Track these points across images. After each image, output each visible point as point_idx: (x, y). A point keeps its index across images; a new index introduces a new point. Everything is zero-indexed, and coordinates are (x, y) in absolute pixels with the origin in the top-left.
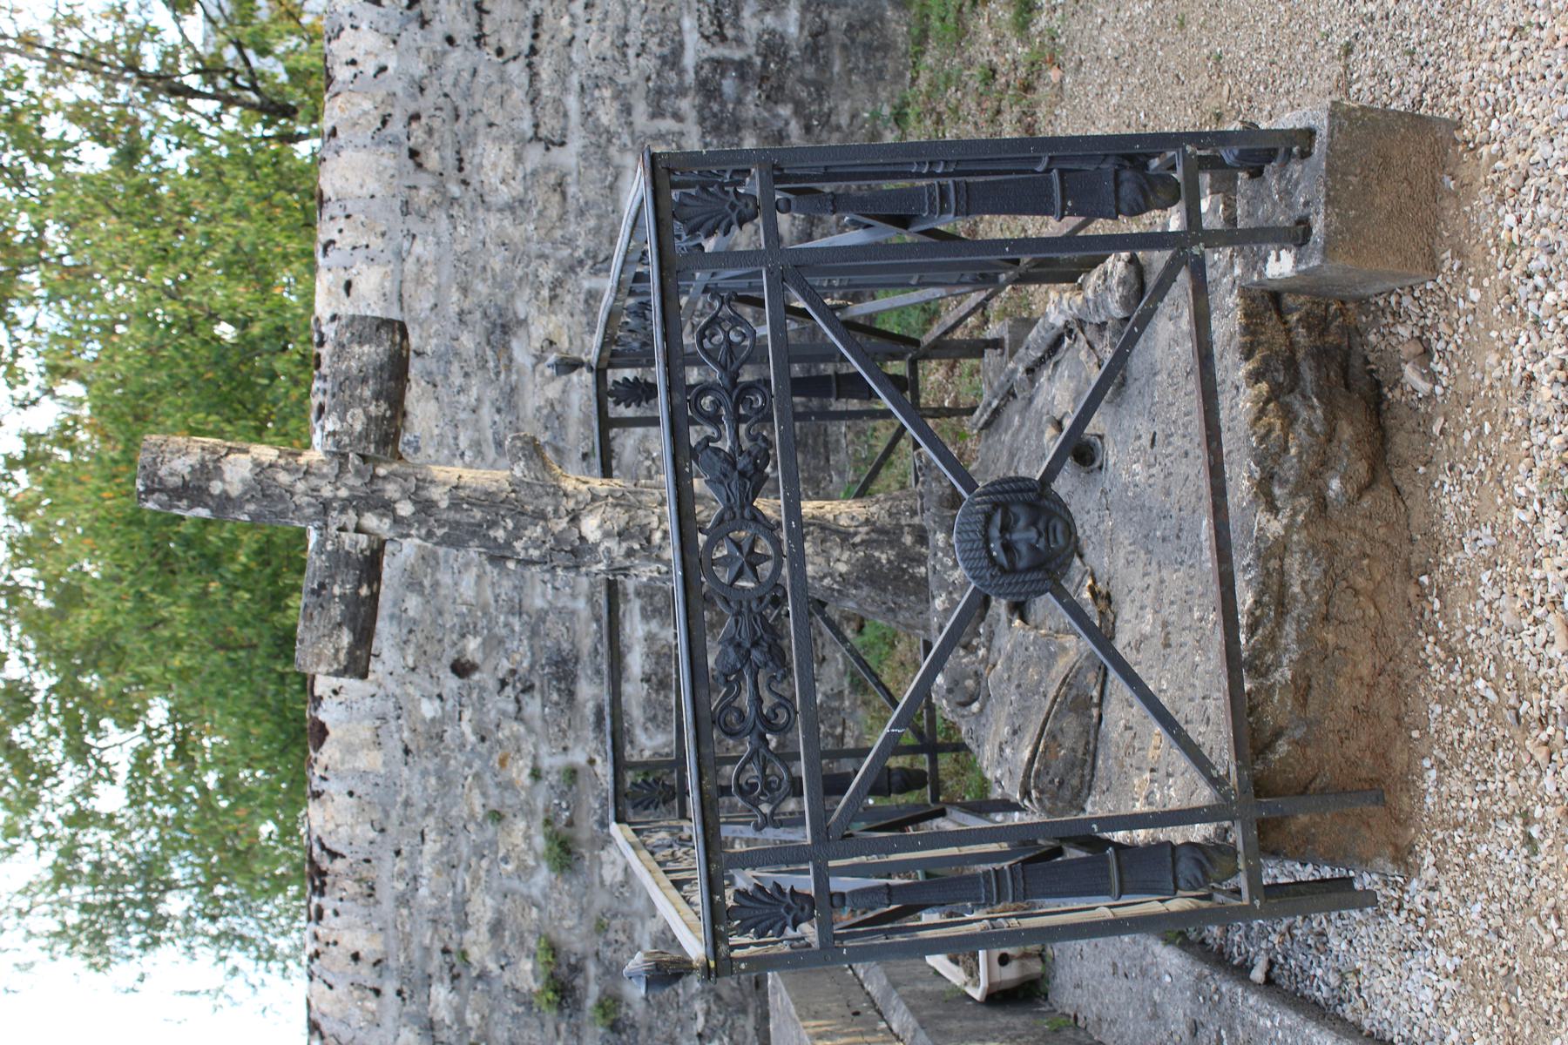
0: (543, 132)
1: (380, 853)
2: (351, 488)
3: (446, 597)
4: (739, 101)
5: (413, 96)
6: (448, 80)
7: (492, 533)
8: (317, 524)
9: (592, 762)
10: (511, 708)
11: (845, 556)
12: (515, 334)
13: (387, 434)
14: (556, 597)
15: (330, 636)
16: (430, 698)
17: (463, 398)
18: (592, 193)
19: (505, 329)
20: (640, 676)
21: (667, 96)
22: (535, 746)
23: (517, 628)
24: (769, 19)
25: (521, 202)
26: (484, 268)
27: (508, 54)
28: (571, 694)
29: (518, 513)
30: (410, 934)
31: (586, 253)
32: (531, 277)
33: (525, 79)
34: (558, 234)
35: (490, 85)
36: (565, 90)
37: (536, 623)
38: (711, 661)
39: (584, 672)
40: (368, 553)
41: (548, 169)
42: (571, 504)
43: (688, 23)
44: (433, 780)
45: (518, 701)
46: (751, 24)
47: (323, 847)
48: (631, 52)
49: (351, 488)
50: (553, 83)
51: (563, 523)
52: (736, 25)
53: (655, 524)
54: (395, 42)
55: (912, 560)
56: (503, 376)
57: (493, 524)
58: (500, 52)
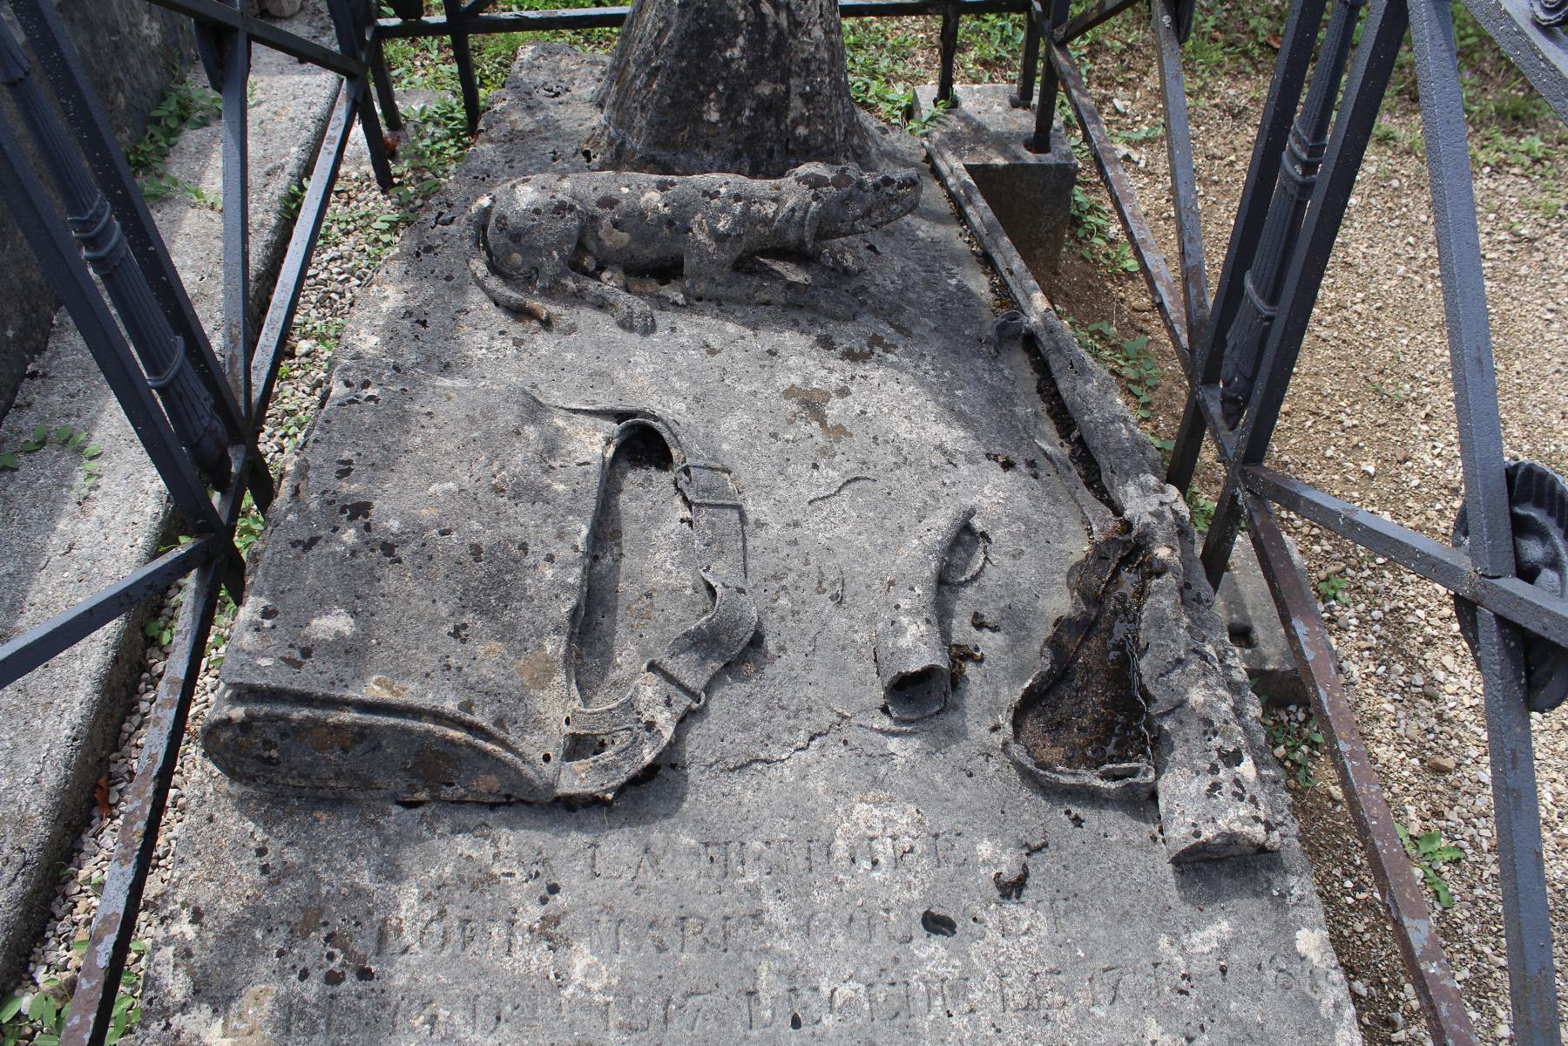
38: (233, 470)
55: (730, 100)
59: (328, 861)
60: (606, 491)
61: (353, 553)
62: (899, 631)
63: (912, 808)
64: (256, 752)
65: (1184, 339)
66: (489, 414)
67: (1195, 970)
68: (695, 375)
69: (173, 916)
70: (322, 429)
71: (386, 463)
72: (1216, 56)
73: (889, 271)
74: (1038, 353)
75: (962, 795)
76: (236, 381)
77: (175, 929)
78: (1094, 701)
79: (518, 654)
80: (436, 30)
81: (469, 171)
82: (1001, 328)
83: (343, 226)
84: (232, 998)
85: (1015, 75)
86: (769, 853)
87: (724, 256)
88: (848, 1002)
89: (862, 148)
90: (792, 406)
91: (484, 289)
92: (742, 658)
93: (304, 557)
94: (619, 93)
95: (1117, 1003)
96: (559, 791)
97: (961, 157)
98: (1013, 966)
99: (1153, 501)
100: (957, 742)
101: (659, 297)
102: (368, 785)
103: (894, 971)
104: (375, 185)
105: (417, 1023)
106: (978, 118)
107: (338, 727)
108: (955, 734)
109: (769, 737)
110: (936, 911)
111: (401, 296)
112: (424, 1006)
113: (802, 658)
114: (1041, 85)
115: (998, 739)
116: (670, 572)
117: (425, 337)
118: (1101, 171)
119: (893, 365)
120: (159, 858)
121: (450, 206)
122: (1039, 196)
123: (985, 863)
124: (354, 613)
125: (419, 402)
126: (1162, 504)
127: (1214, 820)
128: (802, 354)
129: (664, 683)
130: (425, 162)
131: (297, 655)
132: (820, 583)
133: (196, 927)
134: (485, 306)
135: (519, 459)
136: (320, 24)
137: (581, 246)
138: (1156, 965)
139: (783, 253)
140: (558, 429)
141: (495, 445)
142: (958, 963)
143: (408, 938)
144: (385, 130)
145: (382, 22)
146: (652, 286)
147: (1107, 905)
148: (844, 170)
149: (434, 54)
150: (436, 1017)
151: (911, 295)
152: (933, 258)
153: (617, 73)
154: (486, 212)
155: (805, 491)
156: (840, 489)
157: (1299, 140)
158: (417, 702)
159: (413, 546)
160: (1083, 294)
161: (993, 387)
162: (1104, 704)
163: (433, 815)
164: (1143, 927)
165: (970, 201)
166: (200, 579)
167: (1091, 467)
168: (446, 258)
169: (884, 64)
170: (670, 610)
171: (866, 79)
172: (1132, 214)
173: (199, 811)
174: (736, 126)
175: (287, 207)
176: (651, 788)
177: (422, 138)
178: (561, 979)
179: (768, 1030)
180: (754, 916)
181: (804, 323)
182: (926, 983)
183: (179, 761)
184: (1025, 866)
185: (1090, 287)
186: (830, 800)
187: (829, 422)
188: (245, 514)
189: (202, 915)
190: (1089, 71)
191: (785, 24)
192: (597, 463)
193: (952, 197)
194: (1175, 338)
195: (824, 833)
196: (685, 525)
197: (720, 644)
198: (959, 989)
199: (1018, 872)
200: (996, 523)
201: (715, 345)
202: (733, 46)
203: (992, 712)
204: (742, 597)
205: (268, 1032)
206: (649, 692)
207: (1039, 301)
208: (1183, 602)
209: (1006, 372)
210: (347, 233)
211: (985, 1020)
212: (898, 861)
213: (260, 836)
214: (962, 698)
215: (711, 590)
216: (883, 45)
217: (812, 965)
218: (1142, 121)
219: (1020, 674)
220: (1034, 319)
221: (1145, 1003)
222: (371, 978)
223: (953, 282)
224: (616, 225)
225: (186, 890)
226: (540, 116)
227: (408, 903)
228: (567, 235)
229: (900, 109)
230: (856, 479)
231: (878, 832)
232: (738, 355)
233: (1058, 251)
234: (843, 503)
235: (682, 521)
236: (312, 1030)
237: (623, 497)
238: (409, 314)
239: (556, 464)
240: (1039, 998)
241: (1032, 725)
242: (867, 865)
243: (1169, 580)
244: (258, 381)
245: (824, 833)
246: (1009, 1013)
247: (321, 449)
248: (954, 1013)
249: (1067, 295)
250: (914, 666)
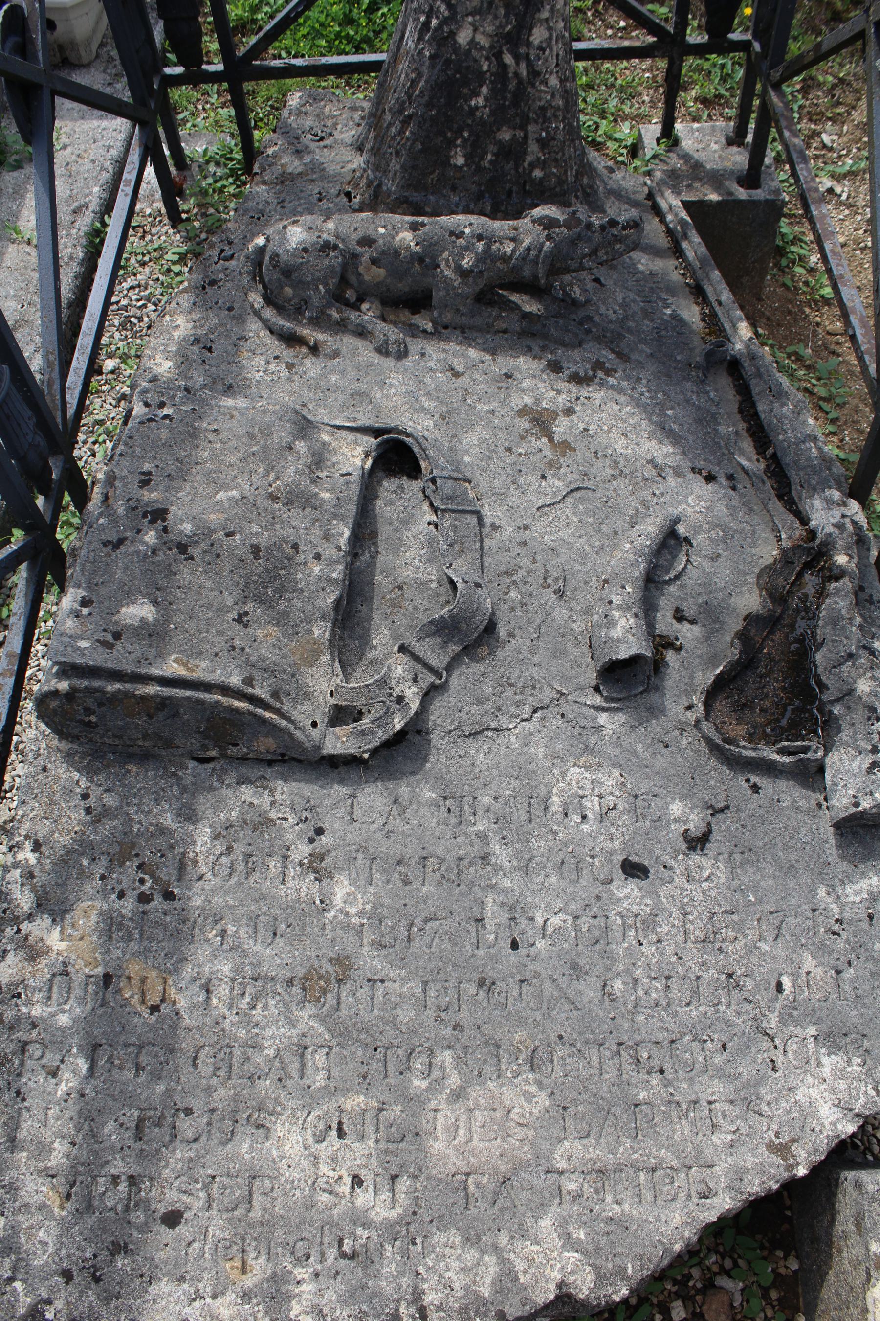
38: (54, 476)
59: (138, 805)
60: (365, 497)
61: (154, 552)
62: (612, 624)
63: (616, 772)
64: (78, 718)
65: (873, 368)
66: (266, 431)
67: (847, 915)
68: (441, 396)
69: (19, 846)
70: (126, 444)
71: (179, 474)
73: (613, 301)
74: (741, 377)
75: (659, 763)
76: (53, 401)
77: (20, 856)
78: (775, 686)
79: (291, 637)
80: (215, 78)
81: (246, 211)
82: (709, 355)
83: (140, 257)
84: (66, 911)
86: (497, 806)
87: (467, 290)
88: (557, 930)
89: (591, 187)
90: (524, 424)
91: (260, 318)
92: (478, 642)
93: (114, 554)
94: (376, 140)
95: (779, 940)
96: (325, 752)
97: (678, 194)
98: (695, 907)
99: (836, 515)
100: (656, 718)
101: (411, 325)
102: (169, 744)
103: (596, 906)
104: (166, 221)
105: (210, 936)
107: (144, 698)
108: (655, 711)
109: (499, 710)
110: (634, 858)
111: (190, 325)
112: (216, 922)
113: (528, 643)
114: (756, 123)
115: (691, 716)
116: (419, 568)
117: (211, 362)
118: (806, 207)
119: (612, 387)
120: (6, 792)
121: (230, 243)
123: (676, 820)
124: (155, 603)
125: (207, 420)
126: (843, 516)
127: (871, 793)
128: (534, 377)
129: (412, 663)
131: (109, 638)
132: (545, 579)
133: (37, 855)
134: (262, 334)
135: (291, 471)
136: (114, 71)
137: (344, 281)
138: (814, 910)
139: (519, 286)
140: (324, 444)
141: (270, 458)
142: (649, 902)
143: (203, 868)
144: (173, 170)
145: (168, 71)
146: (405, 315)
147: (776, 859)
148: (574, 213)
149: (214, 99)
150: (226, 931)
151: (631, 324)
152: (652, 289)
153: (374, 119)
154: (262, 250)
155: (534, 499)
156: (564, 499)
158: (209, 678)
159: (203, 546)
160: (782, 320)
161: (699, 408)
162: (783, 689)
163: (222, 769)
164: (805, 879)
165: (685, 236)
166: (30, 569)
167: (782, 482)
168: (228, 291)
169: (613, 103)
170: (418, 600)
171: (596, 118)
172: (832, 251)
173: (36, 763)
174: (479, 169)
175: (92, 242)
176: (400, 751)
177: (205, 177)
178: (325, 905)
179: (491, 950)
180: (483, 858)
181: (536, 349)
182: (622, 917)
183: (19, 714)
184: (709, 824)
185: (790, 312)
186: (548, 763)
187: (556, 438)
188: (65, 509)
189: (41, 846)
190: (800, 107)
191: (525, 73)
192: (357, 474)
193: (670, 232)
194: (864, 368)
195: (542, 792)
196: (432, 527)
197: (459, 631)
198: (649, 923)
199: (704, 829)
200: (698, 530)
201: (459, 368)
202: (477, 95)
203: (687, 694)
204: (479, 591)
205: (95, 938)
206: (399, 670)
207: (744, 330)
208: (857, 604)
209: (712, 394)
210: (143, 264)
211: (669, 950)
212: (603, 816)
213: (84, 783)
214: (662, 680)
215: (452, 583)
216: (613, 85)
217: (529, 899)
218: (847, 155)
219: (713, 660)
220: (739, 346)
221: (803, 941)
222: (174, 899)
223: (668, 311)
224: (374, 261)
225: (28, 825)
226: (307, 159)
227: (203, 840)
228: (331, 270)
229: (626, 147)
230: (579, 489)
231: (588, 792)
232: (479, 377)
233: (763, 279)
234: (567, 509)
235: (429, 524)
236: (129, 938)
237: (379, 503)
238: (197, 341)
239: (322, 475)
240: (715, 933)
241: (721, 706)
242: (577, 818)
243: (845, 584)
244: (72, 399)
245: (542, 792)
246: (690, 944)
247: (125, 462)
248: (644, 942)
249: (768, 319)
250: (623, 654)
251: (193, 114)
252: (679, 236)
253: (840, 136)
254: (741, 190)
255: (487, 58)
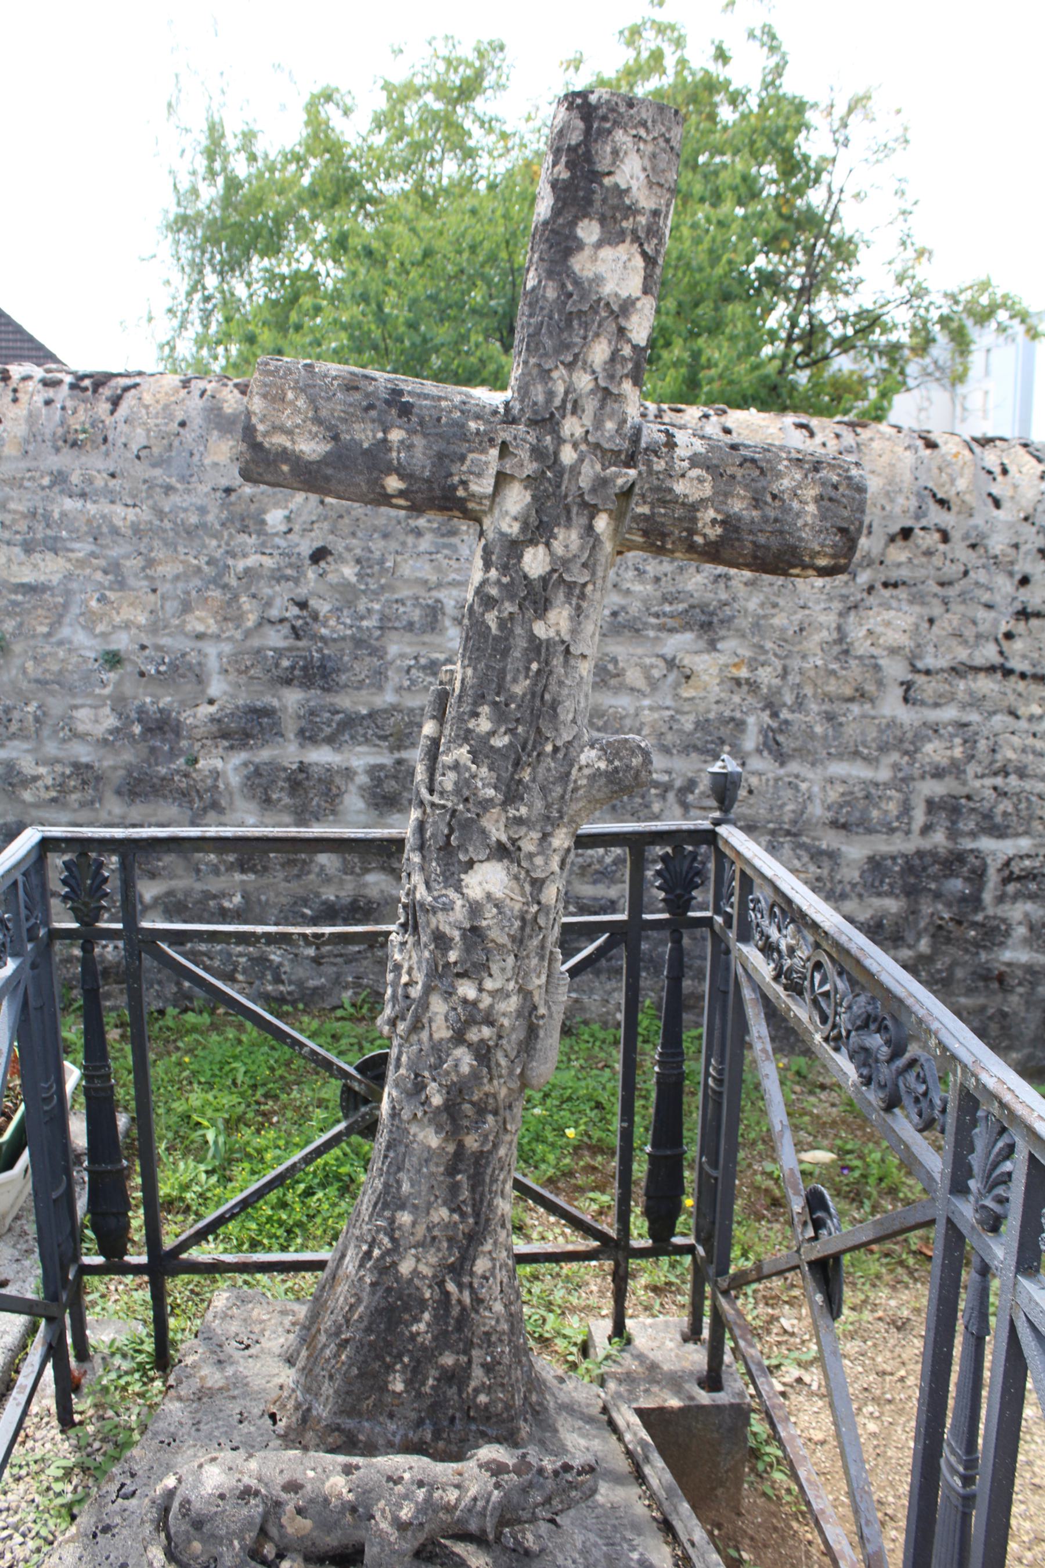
0: (921, 679)
1: (114, 455)
2: (575, 470)
3: (404, 544)
4: (937, 896)
5: (966, 537)
6: (981, 576)
7: (485, 710)
8: (517, 406)
9: (211, 702)
10: (274, 613)
11: (425, 1270)
12: (700, 637)
13: (663, 536)
14: (399, 669)
15: (318, 420)
16: (288, 519)
17: (631, 574)
18: (851, 731)
19: (706, 627)
20: (306, 760)
21: (949, 818)
22: (229, 639)
23: (365, 623)
24: (1022, 931)
25: (846, 652)
26: (775, 605)
27: (1005, 644)
28: (288, 682)
29: (517, 757)
30: (21, 486)
31: (786, 722)
32: (762, 658)
33: (979, 661)
34: (808, 690)
35: (974, 623)
36: (964, 706)
37: (369, 646)
39: (315, 697)
40: (461, 493)
41: (880, 683)
42: (528, 846)
43: (1025, 844)
44: (194, 519)
45: (282, 621)
46: (1018, 911)
47: (127, 389)
48: (999, 781)
49: (575, 470)
50: (971, 693)
51: (498, 833)
52: (1015, 898)
53: (489, 984)
54: (1026, 519)
55: (415, 1371)
56: (653, 620)
57: (500, 715)
58: (1009, 636)
72: (874, 1267)
85: (685, 1300)
89: (541, 1404)
104: (55, 1422)
106: (651, 1355)
114: (710, 1329)
121: (133, 1475)
122: (716, 1435)
130: (108, 1399)
136: (25, 1247)
137: (263, 1532)
144: (72, 1361)
145: (87, 1260)
148: (524, 1456)
154: (171, 1493)
157: (953, 1452)
165: (647, 1460)
171: (543, 1312)
174: (419, 1395)
185: (775, 1529)
193: (629, 1453)
210: (18, 1479)
223: (635, 1556)
224: (300, 1511)
226: (230, 1371)
228: (249, 1521)
249: (752, 1539)
251: (103, 1296)
252: (640, 1459)
253: (799, 1319)
254: (703, 1393)
255: (430, 1286)
